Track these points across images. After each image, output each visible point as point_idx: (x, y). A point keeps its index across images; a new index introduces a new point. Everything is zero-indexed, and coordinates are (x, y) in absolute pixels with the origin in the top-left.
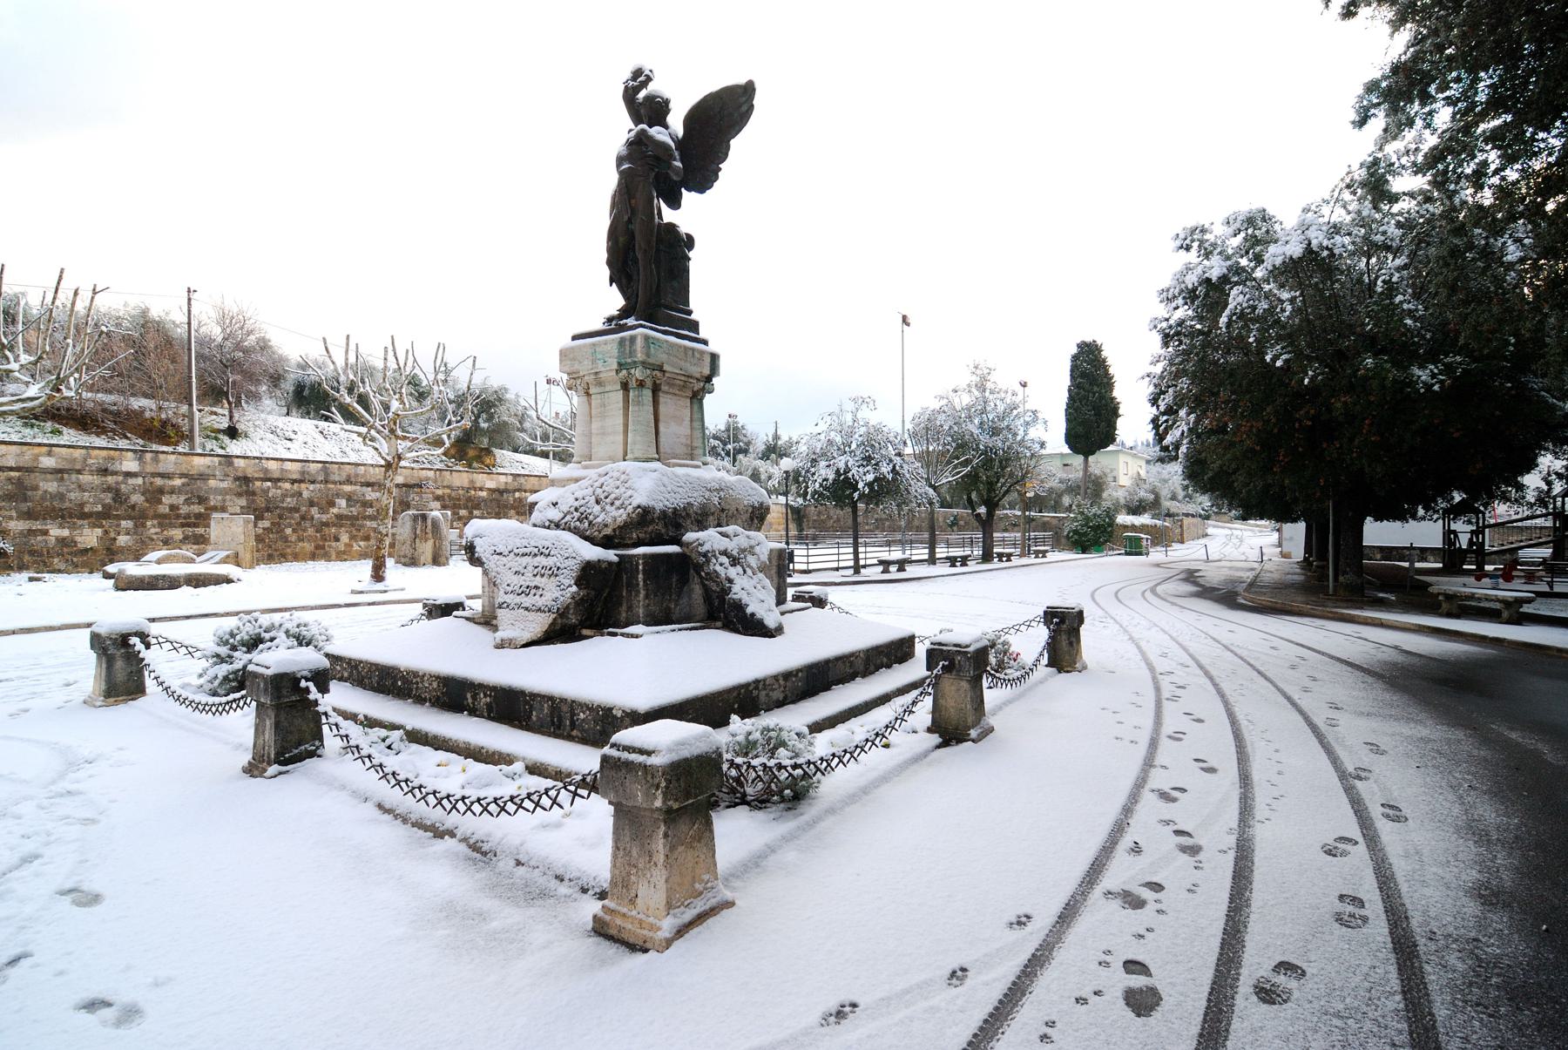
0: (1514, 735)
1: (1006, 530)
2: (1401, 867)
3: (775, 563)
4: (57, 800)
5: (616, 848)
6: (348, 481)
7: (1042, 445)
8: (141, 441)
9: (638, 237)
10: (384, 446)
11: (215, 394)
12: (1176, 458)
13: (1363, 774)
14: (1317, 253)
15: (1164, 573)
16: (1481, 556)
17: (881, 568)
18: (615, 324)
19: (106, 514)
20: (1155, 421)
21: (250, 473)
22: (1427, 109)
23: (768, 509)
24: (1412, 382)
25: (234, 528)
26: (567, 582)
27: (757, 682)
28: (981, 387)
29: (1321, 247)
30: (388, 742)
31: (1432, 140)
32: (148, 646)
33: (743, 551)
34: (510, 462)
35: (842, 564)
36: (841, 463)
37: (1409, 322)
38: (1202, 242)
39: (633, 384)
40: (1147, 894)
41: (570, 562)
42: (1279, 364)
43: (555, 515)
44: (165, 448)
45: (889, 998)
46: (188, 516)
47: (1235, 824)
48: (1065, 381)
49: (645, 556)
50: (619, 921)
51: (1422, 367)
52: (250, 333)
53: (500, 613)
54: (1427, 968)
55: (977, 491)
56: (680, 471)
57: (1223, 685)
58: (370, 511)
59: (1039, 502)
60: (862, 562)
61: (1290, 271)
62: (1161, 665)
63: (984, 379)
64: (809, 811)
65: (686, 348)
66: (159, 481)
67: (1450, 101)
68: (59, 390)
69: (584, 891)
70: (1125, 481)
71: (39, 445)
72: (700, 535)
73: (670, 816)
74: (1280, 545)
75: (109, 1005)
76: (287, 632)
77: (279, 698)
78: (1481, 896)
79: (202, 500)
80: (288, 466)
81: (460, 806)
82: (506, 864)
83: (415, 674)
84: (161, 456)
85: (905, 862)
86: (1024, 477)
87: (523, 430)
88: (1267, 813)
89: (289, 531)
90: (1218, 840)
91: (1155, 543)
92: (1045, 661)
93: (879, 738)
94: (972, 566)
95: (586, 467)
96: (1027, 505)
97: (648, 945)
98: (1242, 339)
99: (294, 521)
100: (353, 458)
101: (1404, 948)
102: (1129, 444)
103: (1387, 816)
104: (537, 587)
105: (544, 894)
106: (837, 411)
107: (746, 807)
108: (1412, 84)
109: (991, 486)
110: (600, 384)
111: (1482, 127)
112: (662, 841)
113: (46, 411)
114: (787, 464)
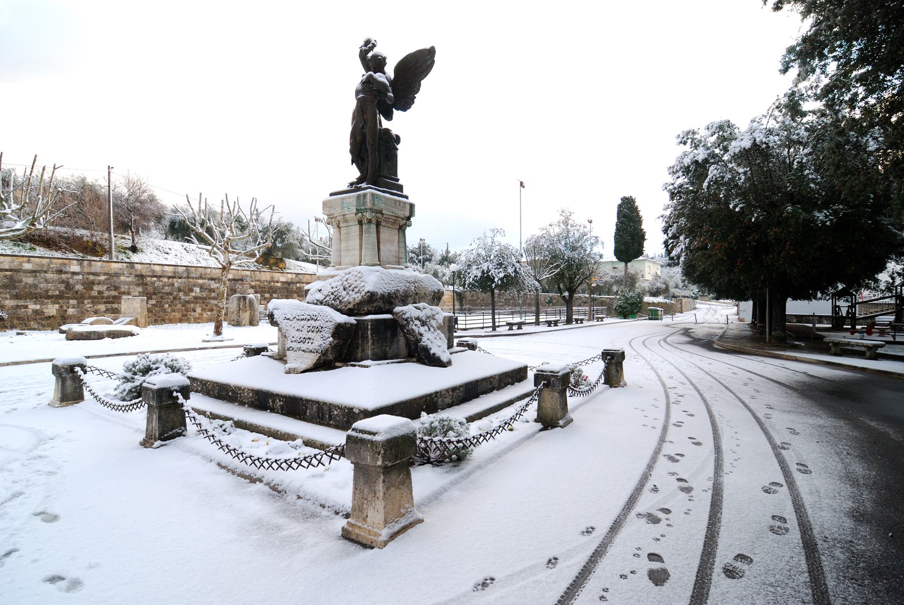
0: (873, 424)
1: (580, 306)
2: (807, 500)
3: (447, 324)
5: (355, 488)
6: (201, 277)
7: (601, 256)
8: (81, 254)
9: (368, 137)
10: (221, 257)
11: (123, 227)
12: (678, 264)
13: (786, 446)
14: (759, 146)
15: (671, 330)
16: (854, 320)
17: (508, 327)
18: (355, 187)
19: (61, 296)
20: (666, 242)
21: (144, 272)
22: (823, 63)
23: (443, 293)
24: (814, 220)
25: (135, 304)
26: (327, 335)
27: (436, 393)
28: (566, 223)
29: (762, 142)
30: (224, 427)
31: (825, 81)
32: (85, 372)
33: (428, 317)
34: (294, 266)
35: (485, 325)
36: (485, 267)
37: (812, 185)
38: (693, 139)
39: (365, 221)
40: (661, 515)
41: (329, 324)
42: (737, 209)
43: (320, 297)
44: (95, 258)
46: (108, 297)
47: (712, 475)
48: (614, 219)
49: (372, 320)
50: (357, 531)
51: (820, 211)
52: (144, 192)
53: (288, 353)
54: (823, 558)
55: (563, 283)
56: (392, 271)
57: (705, 395)
58: (213, 295)
59: (599, 290)
60: (497, 324)
61: (744, 156)
62: (669, 383)
63: (567, 218)
64: (466, 467)
65: (395, 201)
66: (91, 277)
67: (836, 58)
68: (34, 225)
69: (337, 513)
70: (648, 277)
71: (23, 256)
72: (404, 308)
73: (386, 470)
74: (738, 314)
75: (63, 579)
76: (165, 364)
77: (161, 402)
78: (854, 516)
79: (116, 288)
80: (166, 268)
81: (265, 464)
82: (292, 498)
83: (239, 388)
84: (93, 263)
85: (522, 497)
86: (590, 275)
87: (301, 248)
88: (731, 469)
89: (166, 306)
90: (702, 484)
92: (602, 381)
93: (507, 425)
94: (560, 326)
95: (338, 269)
96: (592, 291)
97: (374, 545)
98: (716, 195)
99: (170, 300)
100: (204, 264)
101: (810, 546)
102: (651, 256)
103: (800, 470)
104: (309, 338)
105: (313, 515)
106: (483, 237)
107: (430, 465)
108: (814, 49)
109: (571, 280)
110: (346, 221)
111: (855, 73)
112: (381, 485)
113: (27, 237)
114: (454, 267)
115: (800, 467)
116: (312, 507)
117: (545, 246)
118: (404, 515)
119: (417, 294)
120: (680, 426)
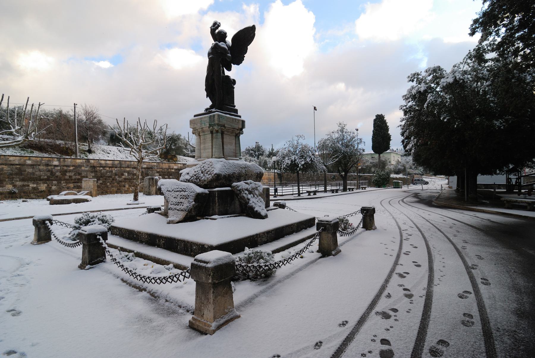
0: (531, 252)
1: (352, 180)
2: (487, 302)
3: (265, 193)
4: (14, 278)
5: (197, 297)
6: (128, 167)
7: (364, 150)
8: (59, 155)
10: (137, 155)
11: (84, 139)
12: (410, 155)
13: (475, 267)
14: (459, 81)
15: (407, 194)
16: (519, 186)
17: (307, 194)
18: (208, 111)
20: (403, 142)
21: (95, 165)
22: (496, 29)
23: (263, 174)
25: (90, 183)
27: (257, 235)
28: (342, 131)
30: (128, 257)
31: (499, 40)
32: (52, 224)
33: (253, 189)
35: (294, 193)
36: (293, 158)
37: (492, 104)
38: (418, 78)
39: (214, 131)
40: (392, 313)
42: (445, 120)
43: (188, 177)
44: (67, 157)
45: (292, 354)
46: (75, 179)
47: (426, 286)
49: (218, 191)
50: (197, 323)
51: (497, 120)
52: (95, 118)
53: (169, 211)
54: (496, 342)
55: (340, 165)
56: (231, 161)
57: (425, 234)
59: (363, 170)
60: (301, 192)
61: (448, 88)
62: (403, 227)
63: (343, 128)
64: (272, 282)
65: (233, 119)
66: (65, 168)
67: (504, 26)
68: (28, 138)
69: (188, 311)
70: (393, 162)
71: (26, 156)
72: (238, 183)
73: (215, 286)
74: (448, 184)
75: (16, 353)
76: (99, 219)
78: (517, 314)
79: (80, 174)
80: (108, 162)
81: (148, 280)
82: (162, 301)
84: (66, 160)
85: (310, 297)
86: (357, 162)
87: (186, 149)
88: (438, 282)
90: (419, 292)
91: (404, 184)
92: (361, 226)
93: (299, 254)
94: (340, 193)
95: (199, 161)
96: (360, 171)
97: (207, 332)
98: (432, 112)
99: (110, 180)
101: (487, 334)
102: (395, 149)
103: (483, 283)
104: (181, 203)
105: (174, 312)
106: (291, 140)
107: (249, 280)
109: (346, 165)
110: (203, 132)
111: (517, 35)
112: (212, 295)
113: (28, 145)
114: (274, 158)
115: (483, 281)
116: (174, 307)
117: (330, 145)
118: (227, 313)
119: (246, 175)
120: (408, 254)
